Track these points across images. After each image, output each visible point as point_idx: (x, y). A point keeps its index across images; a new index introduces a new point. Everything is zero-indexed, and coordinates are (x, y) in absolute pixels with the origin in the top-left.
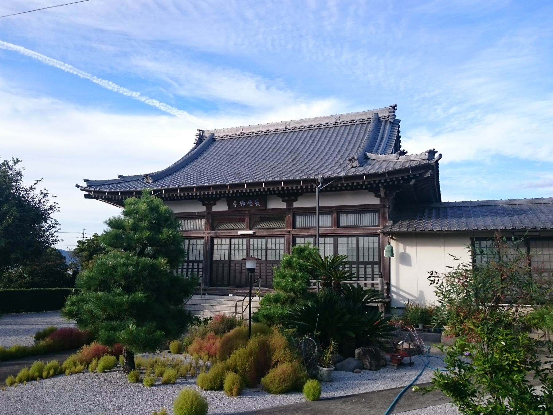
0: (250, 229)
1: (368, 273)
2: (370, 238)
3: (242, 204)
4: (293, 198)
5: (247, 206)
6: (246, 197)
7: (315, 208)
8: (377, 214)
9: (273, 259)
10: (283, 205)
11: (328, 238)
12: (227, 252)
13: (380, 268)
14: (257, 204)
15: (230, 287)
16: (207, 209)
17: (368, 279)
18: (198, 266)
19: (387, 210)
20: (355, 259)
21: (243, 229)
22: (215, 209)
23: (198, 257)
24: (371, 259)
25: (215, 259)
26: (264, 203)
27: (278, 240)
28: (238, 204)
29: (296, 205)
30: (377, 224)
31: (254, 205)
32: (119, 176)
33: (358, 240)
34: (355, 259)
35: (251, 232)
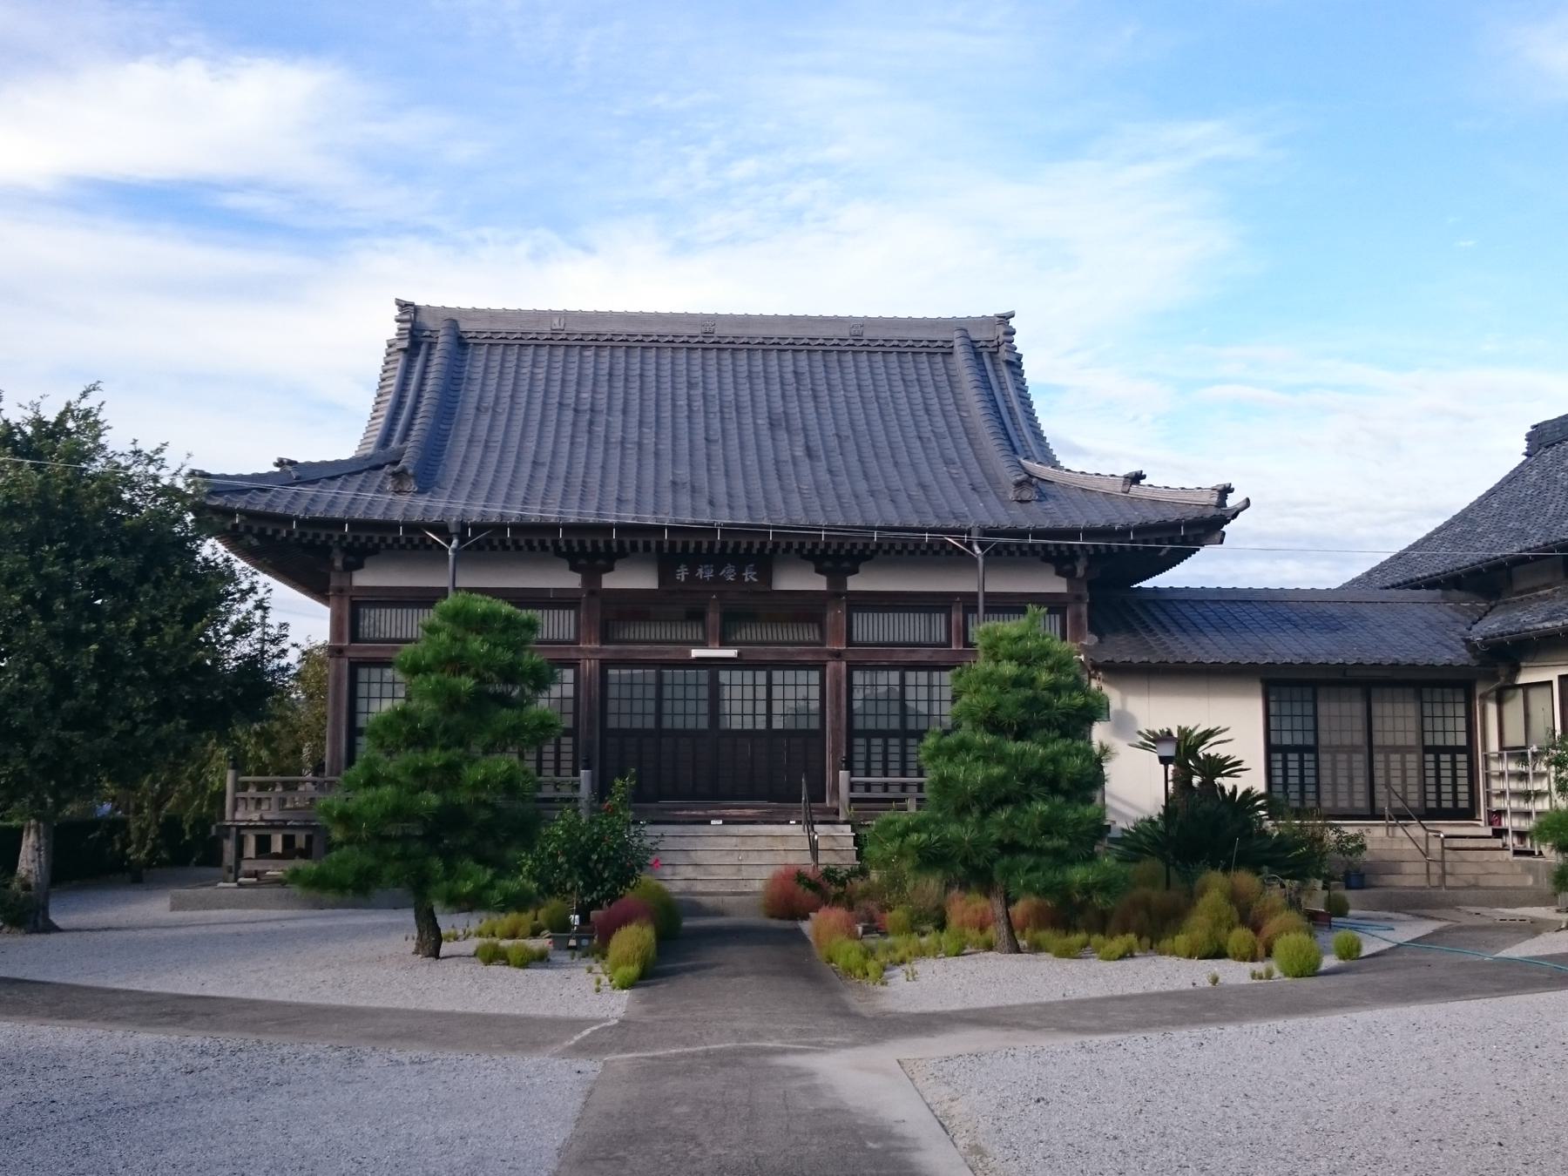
0: (724, 644)
1: (563, 756)
2: (800, 673)
3: (705, 573)
4: (846, 565)
5: (717, 580)
6: (718, 558)
7: (975, 595)
8: (572, 613)
9: (625, 724)
10: (819, 584)
11: (739, 673)
12: (651, 707)
13: (575, 745)
14: (749, 575)
15: (664, 803)
16: (584, 580)
17: (563, 772)
18: (1454, 762)
19: (1084, 609)
20: (895, 724)
21: (703, 644)
22: (610, 582)
23: (748, 720)
24: (882, 725)
25: (612, 723)
26: (766, 575)
27: (802, 674)
28: (693, 571)
29: (855, 584)
30: (943, 639)
31: (739, 577)
32: (280, 463)
33: (903, 679)
34: (895, 724)
35: (731, 653)
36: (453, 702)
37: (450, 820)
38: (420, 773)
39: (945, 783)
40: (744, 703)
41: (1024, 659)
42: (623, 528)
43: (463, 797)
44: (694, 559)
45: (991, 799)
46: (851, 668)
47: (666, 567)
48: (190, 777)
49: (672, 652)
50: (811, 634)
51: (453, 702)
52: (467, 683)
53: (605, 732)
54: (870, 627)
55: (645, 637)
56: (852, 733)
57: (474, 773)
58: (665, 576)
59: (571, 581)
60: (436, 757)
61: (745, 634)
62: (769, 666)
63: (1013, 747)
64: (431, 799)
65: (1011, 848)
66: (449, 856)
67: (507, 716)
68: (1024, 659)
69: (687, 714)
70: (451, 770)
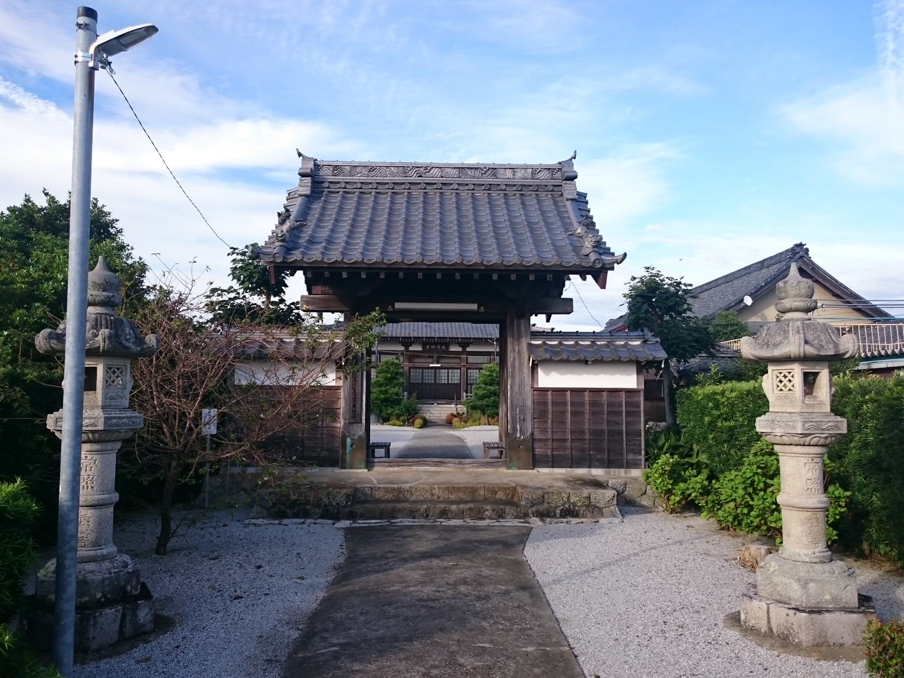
10: (460, 349)
22: (411, 349)
26: (447, 347)
36: (386, 379)
37: (386, 400)
38: (381, 391)
39: (476, 394)
40: (444, 377)
41: (491, 371)
42: (415, 338)
43: (388, 396)
44: (431, 344)
45: (482, 398)
46: (467, 369)
47: (424, 345)
48: (221, 395)
49: (425, 365)
50: (458, 361)
51: (386, 379)
52: (389, 375)
53: (410, 384)
54: (472, 359)
55: (419, 362)
56: (467, 384)
57: (390, 392)
58: (424, 347)
59: (403, 348)
60: (383, 389)
61: (443, 361)
62: (448, 368)
63: (488, 387)
64: (383, 396)
65: (488, 406)
66: (385, 406)
67: (396, 381)
68: (491, 371)
69: (429, 378)
70: (386, 391)
